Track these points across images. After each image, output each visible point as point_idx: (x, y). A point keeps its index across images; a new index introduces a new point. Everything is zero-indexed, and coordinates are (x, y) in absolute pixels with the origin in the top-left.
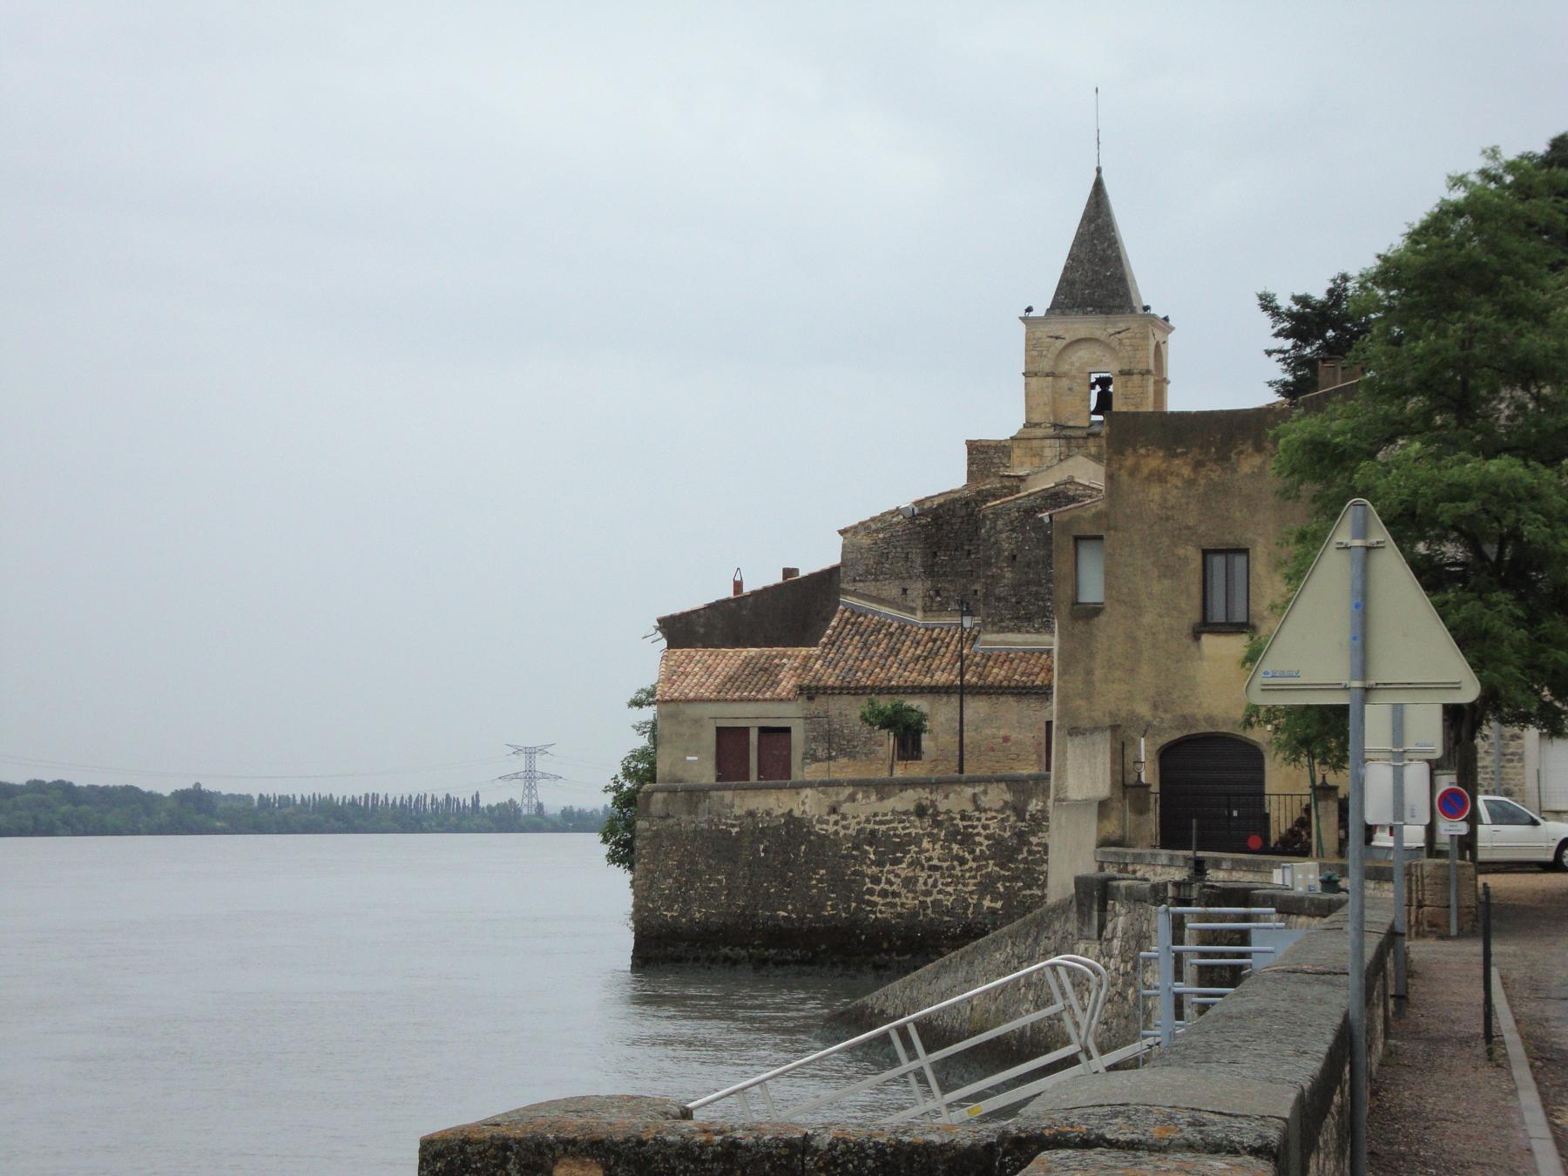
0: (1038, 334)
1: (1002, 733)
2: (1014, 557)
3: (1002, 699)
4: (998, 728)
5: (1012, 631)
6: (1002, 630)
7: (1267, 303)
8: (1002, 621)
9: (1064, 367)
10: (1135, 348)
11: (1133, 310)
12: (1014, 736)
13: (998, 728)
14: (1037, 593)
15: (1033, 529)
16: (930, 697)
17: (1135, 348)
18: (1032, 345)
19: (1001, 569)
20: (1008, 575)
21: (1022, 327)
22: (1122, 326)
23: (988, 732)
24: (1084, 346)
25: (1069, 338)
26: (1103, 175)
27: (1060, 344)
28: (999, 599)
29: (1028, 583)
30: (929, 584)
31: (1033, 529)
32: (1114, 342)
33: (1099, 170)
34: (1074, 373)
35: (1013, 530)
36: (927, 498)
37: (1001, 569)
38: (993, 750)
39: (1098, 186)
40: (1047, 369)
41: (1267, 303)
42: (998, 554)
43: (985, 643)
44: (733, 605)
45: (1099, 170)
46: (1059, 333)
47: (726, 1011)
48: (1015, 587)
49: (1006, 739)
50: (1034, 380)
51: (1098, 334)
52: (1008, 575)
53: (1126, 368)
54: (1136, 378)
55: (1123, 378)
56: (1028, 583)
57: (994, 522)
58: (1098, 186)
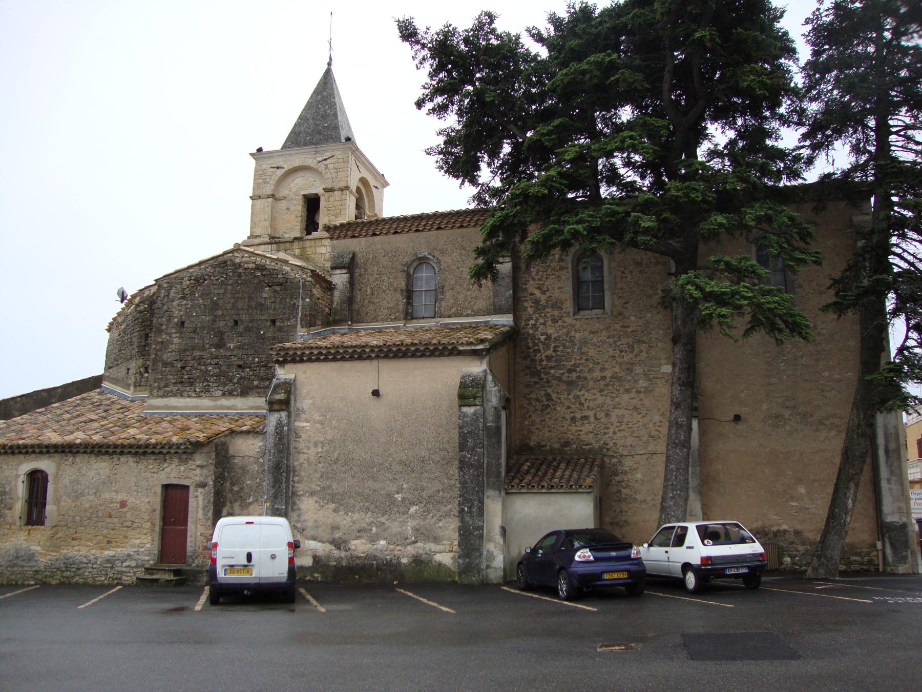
0: (264, 167)
1: (120, 497)
2: (183, 323)
3: (123, 459)
4: (117, 492)
5: (174, 395)
6: (165, 396)
7: (408, 33)
8: (166, 386)
9: (283, 192)
10: (337, 170)
11: (338, 139)
12: (131, 500)
13: (117, 492)
14: (201, 358)
15: (202, 296)
16: (57, 457)
17: (337, 170)
18: (259, 175)
19: (170, 334)
20: (176, 341)
21: (252, 162)
22: (328, 154)
23: (107, 495)
24: (300, 174)
25: (287, 167)
26: (333, 68)
27: (280, 172)
28: (166, 364)
29: (194, 348)
30: (140, 362)
31: (202, 296)
32: (322, 167)
33: (329, 64)
34: (292, 196)
35: (183, 298)
36: (146, 288)
37: (170, 334)
38: (110, 516)
39: (328, 74)
40: (269, 192)
41: (408, 33)
42: (170, 319)
43: (151, 407)
44: (45, 394)
45: (329, 64)
46: (280, 164)
47: (271, 609)
48: (182, 351)
49: (123, 504)
50: (258, 202)
51: (310, 161)
52: (176, 341)
53: (329, 186)
54: (337, 193)
55: (327, 194)
56: (194, 348)
57: (168, 291)
58: (328, 74)
